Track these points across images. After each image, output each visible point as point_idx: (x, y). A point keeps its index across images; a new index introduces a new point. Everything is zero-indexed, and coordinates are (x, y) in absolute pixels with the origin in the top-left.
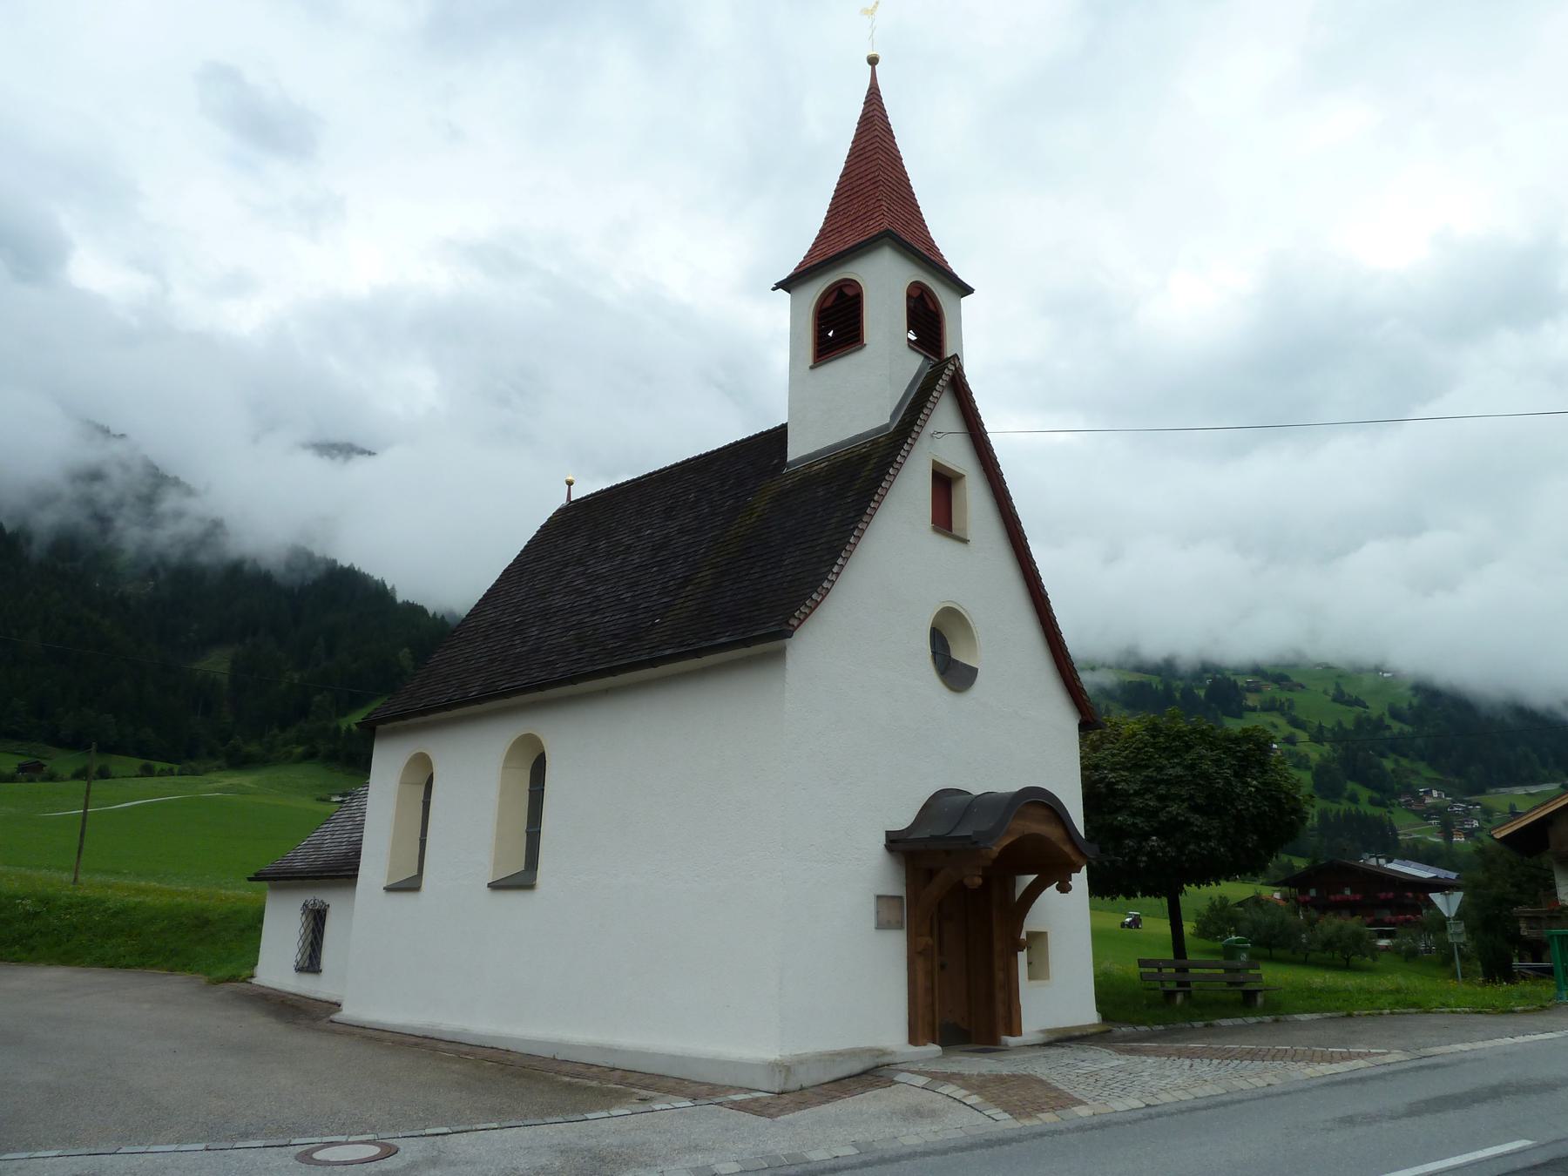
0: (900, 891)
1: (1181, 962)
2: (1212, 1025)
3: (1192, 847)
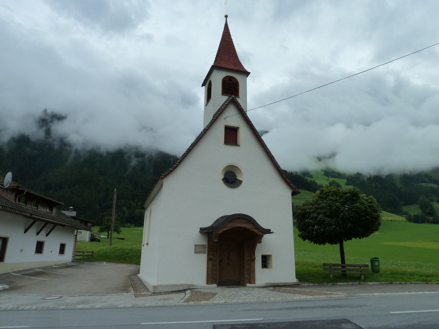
0: (206, 243)
1: (343, 265)
2: (360, 284)
3: (327, 228)
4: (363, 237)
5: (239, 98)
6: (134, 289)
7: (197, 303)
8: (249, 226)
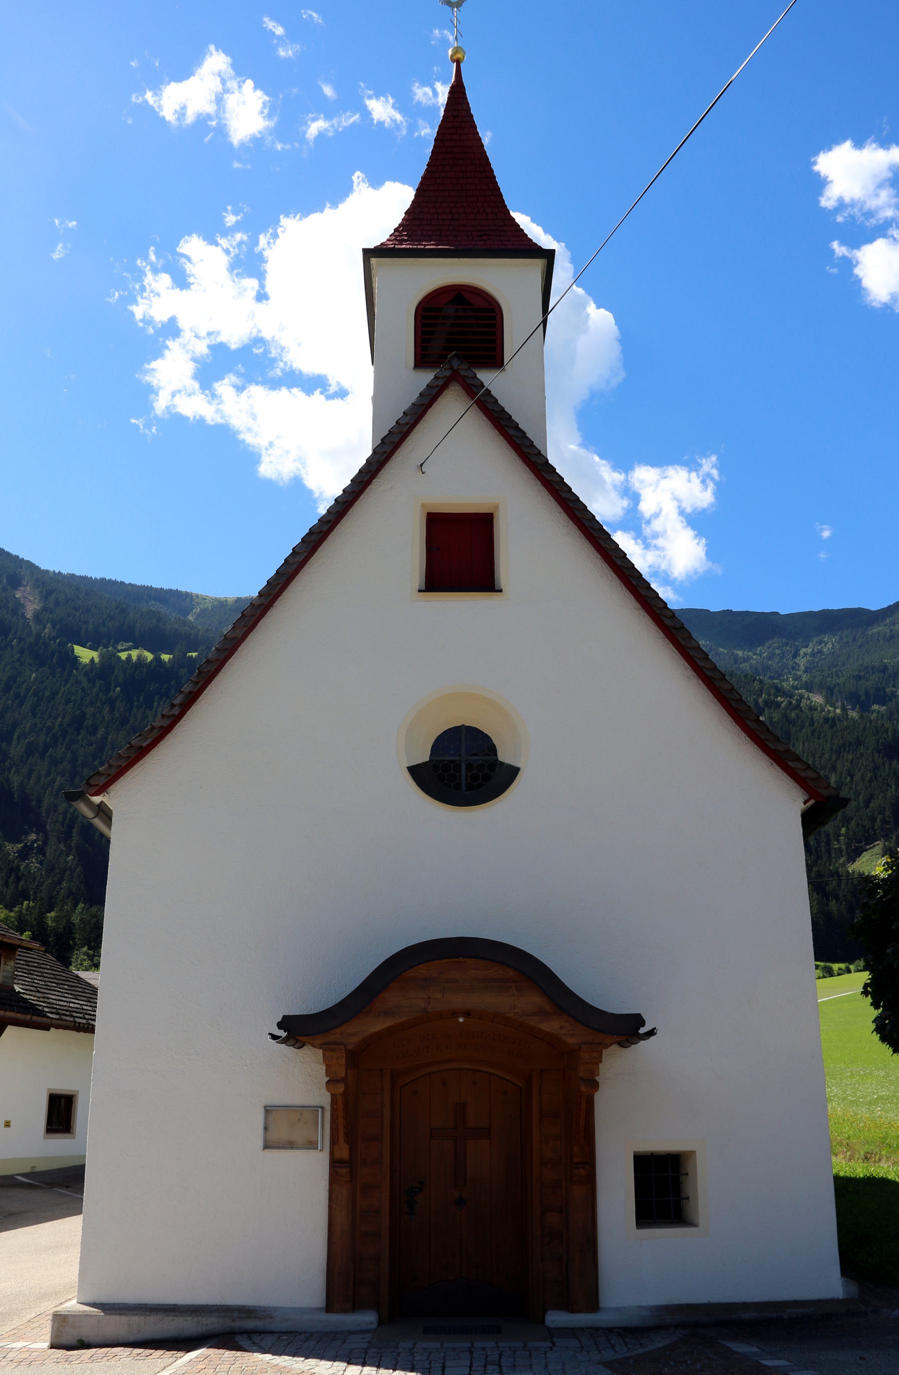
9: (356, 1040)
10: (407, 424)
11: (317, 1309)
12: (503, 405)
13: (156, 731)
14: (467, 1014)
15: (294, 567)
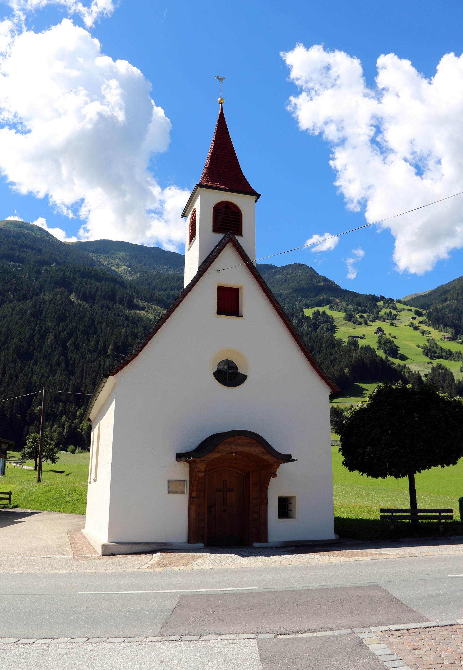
4: (448, 465)
5: (242, 237)
6: (74, 549)
7: (168, 569)
8: (257, 450)
9: (210, 459)
10: (215, 256)
11: (185, 543)
12: (246, 253)
13: (133, 355)
14: (236, 453)
15: (178, 302)
